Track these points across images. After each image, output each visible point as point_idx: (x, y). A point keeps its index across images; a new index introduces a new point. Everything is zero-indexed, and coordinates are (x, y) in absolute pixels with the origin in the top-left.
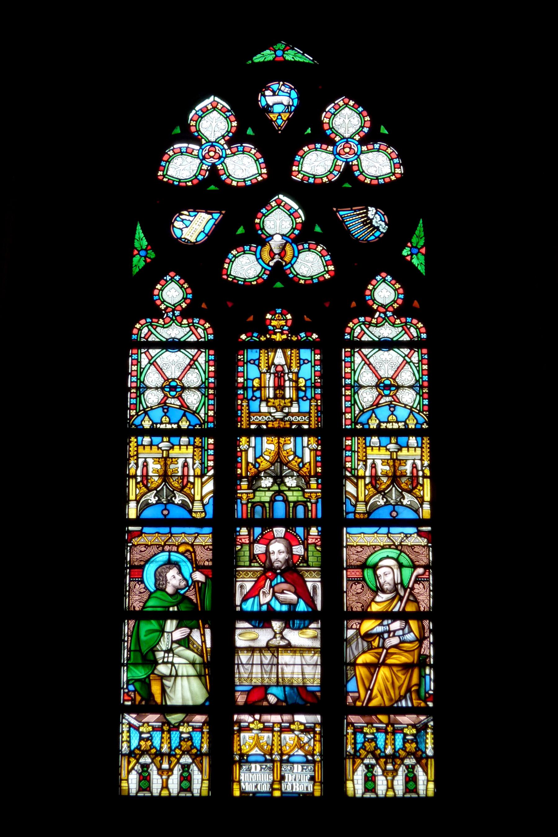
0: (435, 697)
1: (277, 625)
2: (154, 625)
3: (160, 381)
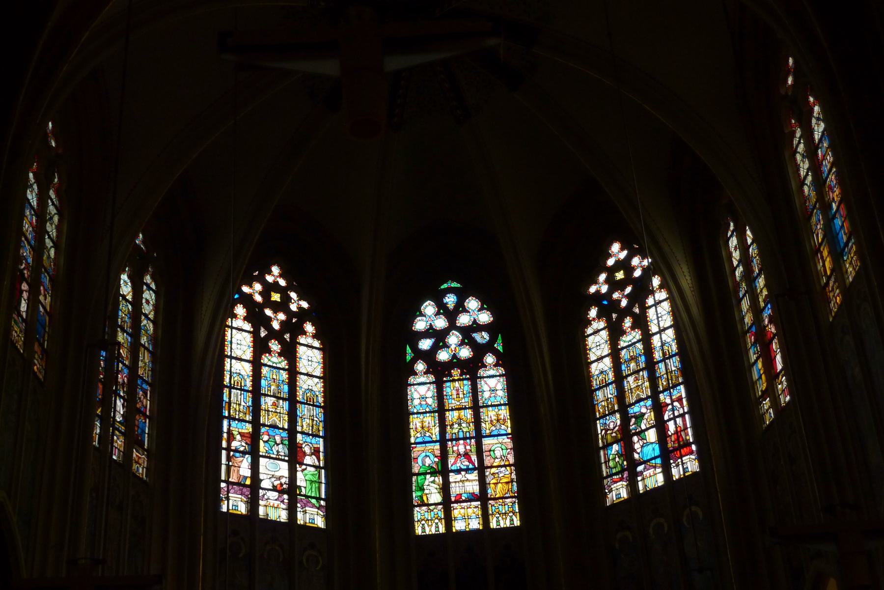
0: (517, 492)
1: (463, 473)
2: (423, 477)
3: (418, 396)
